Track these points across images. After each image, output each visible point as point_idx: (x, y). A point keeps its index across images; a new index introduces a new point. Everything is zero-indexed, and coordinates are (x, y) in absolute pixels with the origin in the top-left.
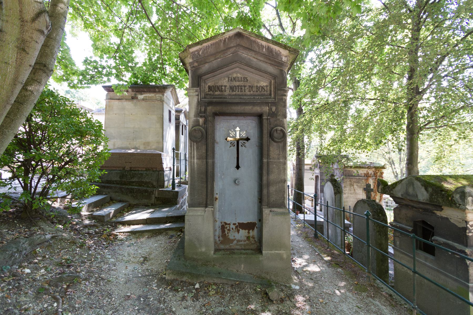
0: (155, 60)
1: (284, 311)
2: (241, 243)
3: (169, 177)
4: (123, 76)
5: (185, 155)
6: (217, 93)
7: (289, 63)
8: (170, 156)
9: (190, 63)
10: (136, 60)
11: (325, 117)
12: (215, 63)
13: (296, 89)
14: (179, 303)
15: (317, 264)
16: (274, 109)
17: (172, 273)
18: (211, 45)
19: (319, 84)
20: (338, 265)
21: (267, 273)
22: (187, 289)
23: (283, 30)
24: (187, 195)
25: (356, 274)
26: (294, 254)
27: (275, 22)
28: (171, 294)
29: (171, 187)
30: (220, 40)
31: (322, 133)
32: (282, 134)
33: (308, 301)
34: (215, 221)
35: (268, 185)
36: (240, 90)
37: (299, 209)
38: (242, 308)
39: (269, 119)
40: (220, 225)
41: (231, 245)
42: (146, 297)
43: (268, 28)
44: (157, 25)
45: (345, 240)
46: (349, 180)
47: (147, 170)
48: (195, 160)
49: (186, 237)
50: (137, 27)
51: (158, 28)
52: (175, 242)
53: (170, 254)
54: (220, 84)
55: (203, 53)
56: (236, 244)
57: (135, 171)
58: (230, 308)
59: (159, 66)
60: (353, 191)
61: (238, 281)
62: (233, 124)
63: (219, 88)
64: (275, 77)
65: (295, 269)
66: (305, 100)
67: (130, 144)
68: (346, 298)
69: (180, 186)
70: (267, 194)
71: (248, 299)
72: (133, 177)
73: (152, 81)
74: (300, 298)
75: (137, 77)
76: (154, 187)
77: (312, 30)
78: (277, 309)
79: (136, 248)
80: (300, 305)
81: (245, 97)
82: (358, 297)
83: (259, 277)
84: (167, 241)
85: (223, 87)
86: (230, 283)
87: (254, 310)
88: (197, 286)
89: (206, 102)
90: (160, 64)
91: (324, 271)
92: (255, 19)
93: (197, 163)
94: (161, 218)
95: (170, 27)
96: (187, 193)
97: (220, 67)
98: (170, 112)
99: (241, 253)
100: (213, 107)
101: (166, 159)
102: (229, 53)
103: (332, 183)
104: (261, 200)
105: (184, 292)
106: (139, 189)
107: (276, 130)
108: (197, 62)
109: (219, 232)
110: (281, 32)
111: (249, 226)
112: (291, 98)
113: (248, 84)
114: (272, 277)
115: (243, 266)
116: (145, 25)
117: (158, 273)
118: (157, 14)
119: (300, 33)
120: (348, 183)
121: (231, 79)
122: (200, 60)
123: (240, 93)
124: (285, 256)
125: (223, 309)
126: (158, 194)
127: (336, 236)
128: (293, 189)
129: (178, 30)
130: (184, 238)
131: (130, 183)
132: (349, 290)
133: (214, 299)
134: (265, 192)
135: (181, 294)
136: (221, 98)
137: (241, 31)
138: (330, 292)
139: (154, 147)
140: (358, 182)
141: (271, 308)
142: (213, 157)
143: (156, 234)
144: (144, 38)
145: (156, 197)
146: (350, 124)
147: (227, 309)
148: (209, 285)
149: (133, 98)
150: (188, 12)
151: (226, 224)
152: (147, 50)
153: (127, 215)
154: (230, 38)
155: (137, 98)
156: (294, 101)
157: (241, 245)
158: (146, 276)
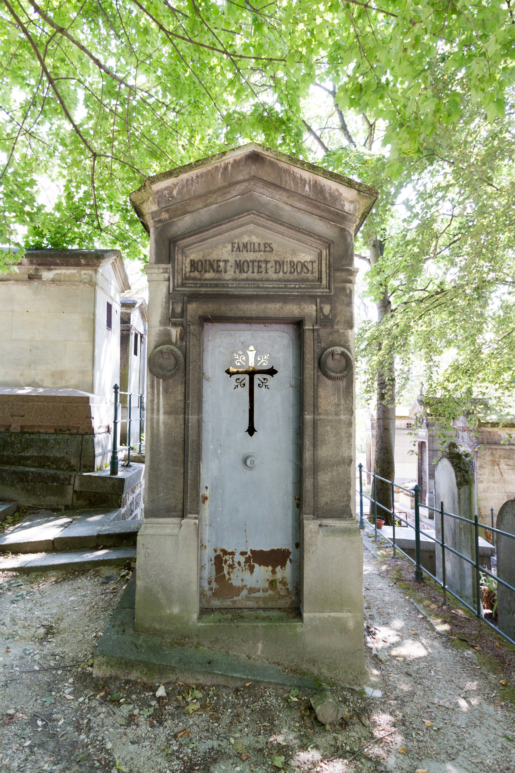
0: (80, 199)
1: (348, 748)
2: (257, 595)
3: (104, 448)
4: (11, 233)
5: (141, 398)
6: (208, 275)
7: (358, 214)
8: (108, 401)
9: (152, 213)
10: (40, 200)
11: (439, 318)
12: (205, 214)
13: (377, 260)
14: (121, 730)
15: (420, 641)
16: (327, 309)
17: (108, 663)
18: (197, 177)
19: (424, 252)
20: (465, 641)
21: (314, 662)
22: (139, 699)
23: (349, 138)
24: (143, 487)
25: (504, 663)
26: (372, 617)
27: (332, 127)
28: (104, 710)
29: (109, 468)
30: (217, 167)
31: (431, 350)
32: (343, 362)
33: (401, 724)
34: (202, 546)
35: (315, 469)
36: (256, 270)
37: (383, 514)
38: (257, 742)
39: (318, 330)
40: (213, 555)
41: (235, 598)
42: (49, 719)
43: (318, 133)
44: (86, 127)
45: (479, 585)
46: (488, 453)
47: (58, 431)
48: (162, 417)
49: (139, 583)
50: (43, 130)
51: (88, 133)
52: (114, 592)
53: (104, 620)
54: (214, 256)
55: (180, 192)
56: (247, 597)
57: (33, 433)
58: (232, 741)
59: (88, 211)
60: (497, 477)
61: (250, 680)
62: (242, 339)
63: (213, 265)
64: (329, 244)
65: (374, 652)
66: (394, 283)
67: (22, 375)
68: (482, 716)
69: (128, 466)
70: (311, 493)
71: (271, 721)
72: (28, 446)
73: (72, 241)
74: (383, 719)
75: (40, 234)
76: (71, 468)
77: (406, 147)
78: (333, 743)
79: (29, 605)
80: (382, 733)
81: (267, 285)
82: (508, 714)
83: (295, 671)
84: (98, 590)
85: (222, 264)
86: (232, 684)
87: (284, 747)
88: (161, 692)
89: (184, 295)
90: (91, 207)
91: (436, 656)
92: (289, 119)
93: (165, 424)
94: (85, 537)
95: (113, 131)
96: (143, 481)
97: (215, 223)
98: (109, 307)
99: (257, 618)
100: (201, 303)
101: (99, 408)
102: (234, 193)
103: (452, 463)
104: (299, 502)
105: (131, 706)
106: (40, 474)
107: (333, 354)
108: (167, 211)
109: (209, 571)
110: (345, 142)
111: (273, 558)
112: (365, 279)
113: (272, 257)
114: (324, 671)
115: (260, 645)
116: (59, 127)
117: (76, 662)
118: (87, 106)
119: (381, 150)
120: (488, 458)
121: (239, 247)
122: (173, 207)
123: (256, 276)
124: (351, 624)
125: (215, 743)
126: (81, 485)
127: (462, 577)
128: (372, 473)
129: (129, 138)
130: (134, 583)
131: (21, 461)
132: (491, 701)
133: (196, 721)
134: (308, 483)
135: (125, 710)
136: (217, 286)
137: (259, 150)
138: (447, 704)
139: (73, 382)
140: (509, 458)
141: (320, 740)
142: (199, 410)
143: (74, 574)
144: (57, 154)
145: (75, 492)
146: (489, 335)
147: (224, 743)
148: (188, 688)
149: (31, 278)
150: (151, 101)
151: (225, 552)
152: (64, 177)
153: (13, 532)
154: (236, 163)
155: (40, 278)
156: (371, 285)
157: (257, 599)
158: (50, 669)
